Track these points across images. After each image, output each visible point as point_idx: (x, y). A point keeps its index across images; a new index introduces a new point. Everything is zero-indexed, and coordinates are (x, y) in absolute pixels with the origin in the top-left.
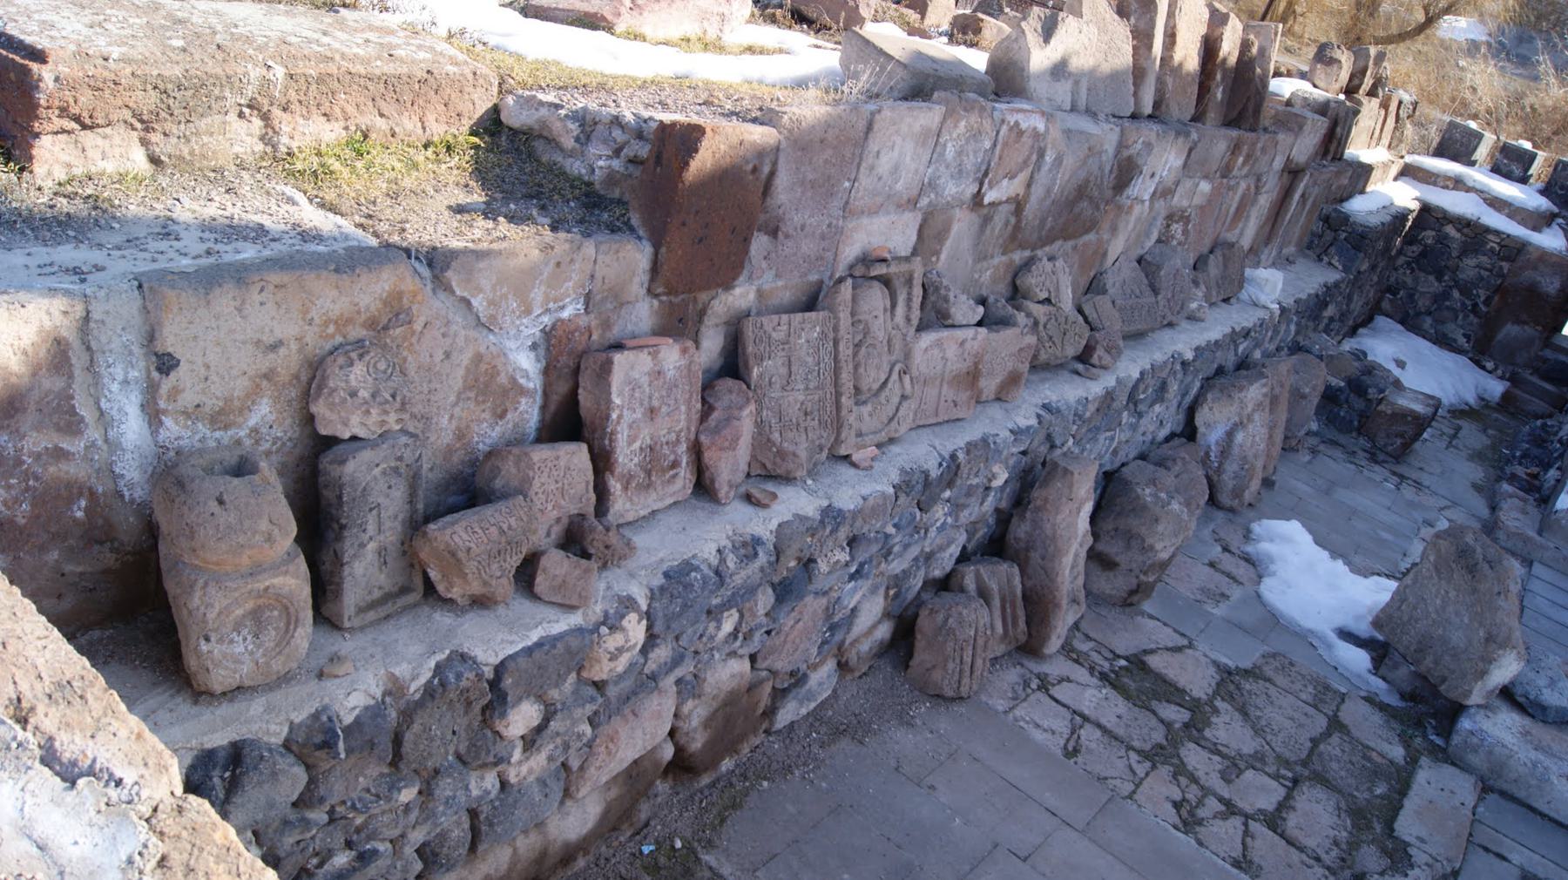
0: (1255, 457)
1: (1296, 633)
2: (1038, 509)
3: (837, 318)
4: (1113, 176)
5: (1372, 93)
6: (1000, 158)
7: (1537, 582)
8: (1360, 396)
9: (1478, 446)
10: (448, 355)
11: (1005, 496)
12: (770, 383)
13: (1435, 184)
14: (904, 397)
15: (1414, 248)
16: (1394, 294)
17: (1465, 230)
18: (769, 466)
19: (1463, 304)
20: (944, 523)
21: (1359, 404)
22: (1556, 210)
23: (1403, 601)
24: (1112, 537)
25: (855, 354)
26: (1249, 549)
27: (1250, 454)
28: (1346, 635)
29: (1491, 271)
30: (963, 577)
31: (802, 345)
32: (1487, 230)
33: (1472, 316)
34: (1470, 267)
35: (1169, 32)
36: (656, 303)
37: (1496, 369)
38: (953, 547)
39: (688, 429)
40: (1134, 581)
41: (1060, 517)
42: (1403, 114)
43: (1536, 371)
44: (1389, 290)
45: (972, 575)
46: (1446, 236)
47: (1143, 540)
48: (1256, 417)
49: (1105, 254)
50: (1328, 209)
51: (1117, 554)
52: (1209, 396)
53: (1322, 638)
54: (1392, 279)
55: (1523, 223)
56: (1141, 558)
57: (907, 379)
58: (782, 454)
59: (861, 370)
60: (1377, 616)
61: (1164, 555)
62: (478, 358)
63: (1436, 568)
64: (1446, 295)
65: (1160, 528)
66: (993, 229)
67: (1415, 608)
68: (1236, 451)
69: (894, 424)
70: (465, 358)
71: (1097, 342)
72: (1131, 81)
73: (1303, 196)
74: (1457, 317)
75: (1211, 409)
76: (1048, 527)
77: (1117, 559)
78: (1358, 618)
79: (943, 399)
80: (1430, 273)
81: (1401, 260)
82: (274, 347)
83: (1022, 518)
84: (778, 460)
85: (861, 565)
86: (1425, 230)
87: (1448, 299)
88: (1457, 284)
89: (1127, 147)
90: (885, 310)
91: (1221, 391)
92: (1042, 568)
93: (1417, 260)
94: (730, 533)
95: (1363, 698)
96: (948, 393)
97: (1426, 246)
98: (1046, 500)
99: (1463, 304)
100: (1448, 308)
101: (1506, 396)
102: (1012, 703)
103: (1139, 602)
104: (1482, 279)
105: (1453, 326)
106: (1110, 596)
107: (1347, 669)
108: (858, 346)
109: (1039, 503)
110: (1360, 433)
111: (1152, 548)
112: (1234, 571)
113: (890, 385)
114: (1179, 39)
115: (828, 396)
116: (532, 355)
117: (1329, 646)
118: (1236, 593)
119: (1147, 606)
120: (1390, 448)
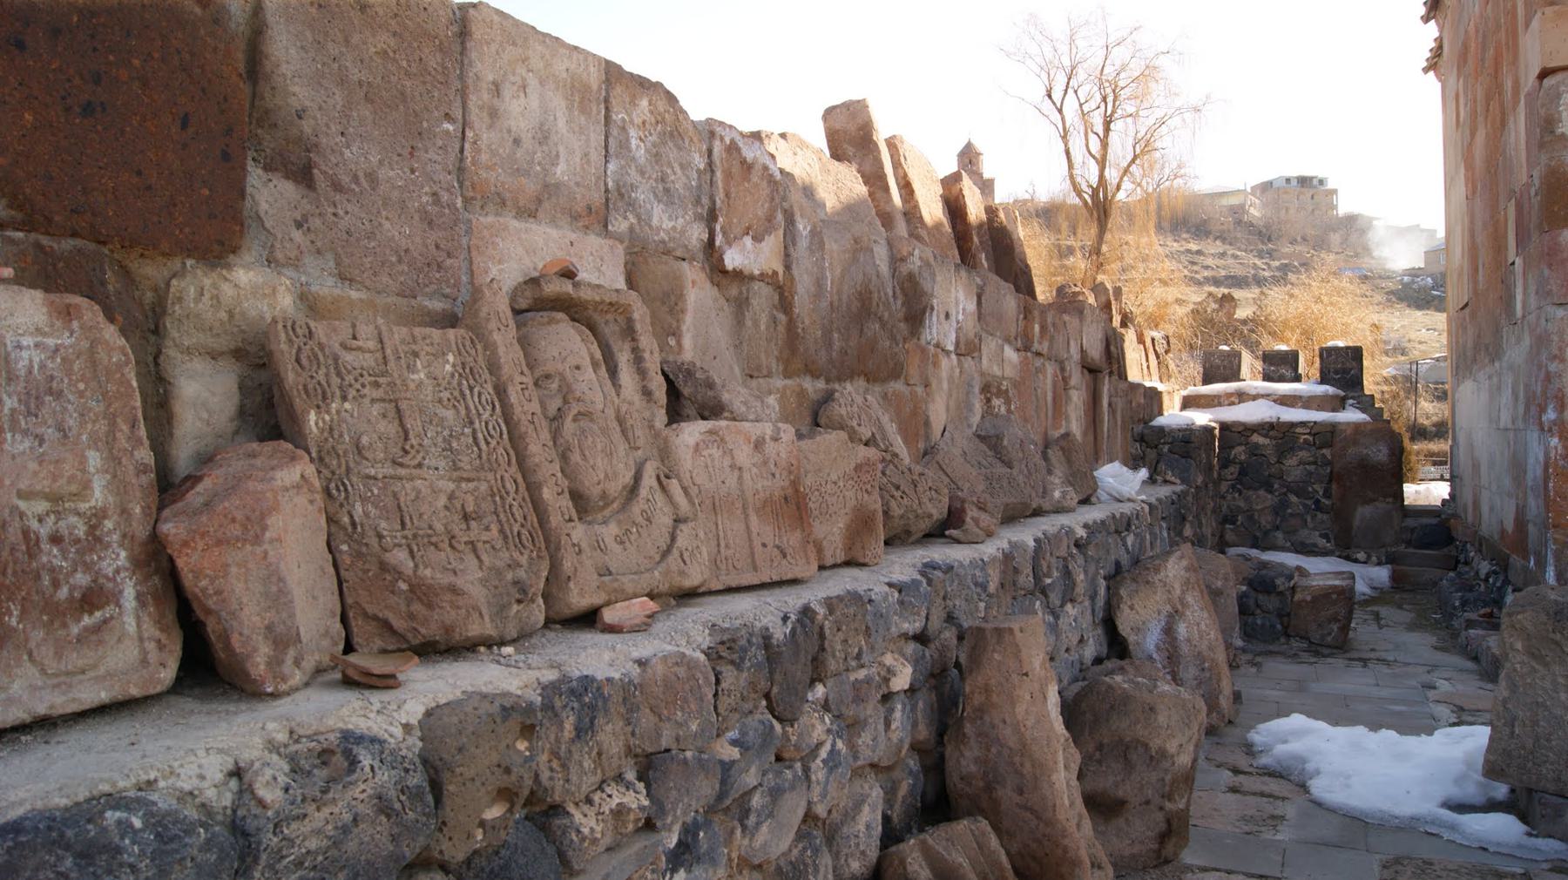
0: (1211, 648)
1: (1399, 829)
2: (981, 711)
3: (490, 347)
4: (899, 302)
5: (1124, 324)
6: (727, 195)
8: (1269, 593)
9: (1408, 620)
11: (920, 715)
12: (359, 449)
13: (1220, 405)
14: (677, 521)
15: (1232, 469)
16: (1234, 523)
17: (1271, 433)
18: (398, 624)
19: (1305, 506)
20: (833, 752)
21: (1271, 602)
22: (1342, 393)
23: (1511, 723)
24: (1099, 762)
25: (556, 435)
26: (1264, 760)
27: (1204, 647)
28: (1461, 808)
29: (1315, 463)
30: (903, 862)
31: (420, 385)
32: (1292, 425)
33: (1319, 515)
34: (1293, 466)
35: (903, 183)
37: (1369, 557)
38: (866, 809)
39: (124, 511)
40: (1160, 816)
41: (1020, 709)
42: (1161, 350)
43: (1409, 543)
44: (1225, 520)
45: (916, 854)
46: (1257, 446)
47: (1146, 746)
48: (1189, 599)
49: (927, 423)
50: (1139, 428)
51: (1116, 785)
52: (1123, 592)
53: (1434, 821)
54: (1224, 509)
55: (1320, 408)
56: (1154, 777)
57: (674, 486)
58: (421, 592)
59: (576, 457)
60: (1487, 761)
61: (1184, 759)
63: (1533, 655)
64: (1284, 504)
65: (1162, 719)
66: (756, 323)
67: (1535, 723)
68: (1185, 649)
69: (673, 560)
71: (963, 501)
72: (879, 223)
73: (1110, 405)
74: (1306, 521)
75: (1132, 608)
76: (1007, 732)
77: (1120, 793)
78: (1459, 780)
79: (757, 543)
80: (1260, 487)
81: (1224, 487)
83: (961, 738)
84: (417, 607)
85: (690, 832)
86: (1233, 447)
87: (1288, 507)
88: (1290, 490)
89: (903, 260)
90: (595, 365)
91: (1134, 580)
92: (1026, 808)
93: (1239, 480)
94: (282, 737)
95: (1551, 870)
96: (763, 530)
97: (1241, 463)
98: (987, 690)
99: (1305, 506)
100: (1291, 515)
101: (1395, 577)
103: (1176, 855)
104: (1310, 473)
105: (1306, 532)
106: (1133, 856)
107: (1499, 844)
108: (556, 419)
109: (978, 699)
110: (1288, 636)
111: (1163, 753)
112: (1266, 789)
113: (643, 492)
114: (916, 186)
115: (510, 486)
117: (1453, 827)
118: (1290, 810)
119: (1188, 857)
120: (1329, 639)
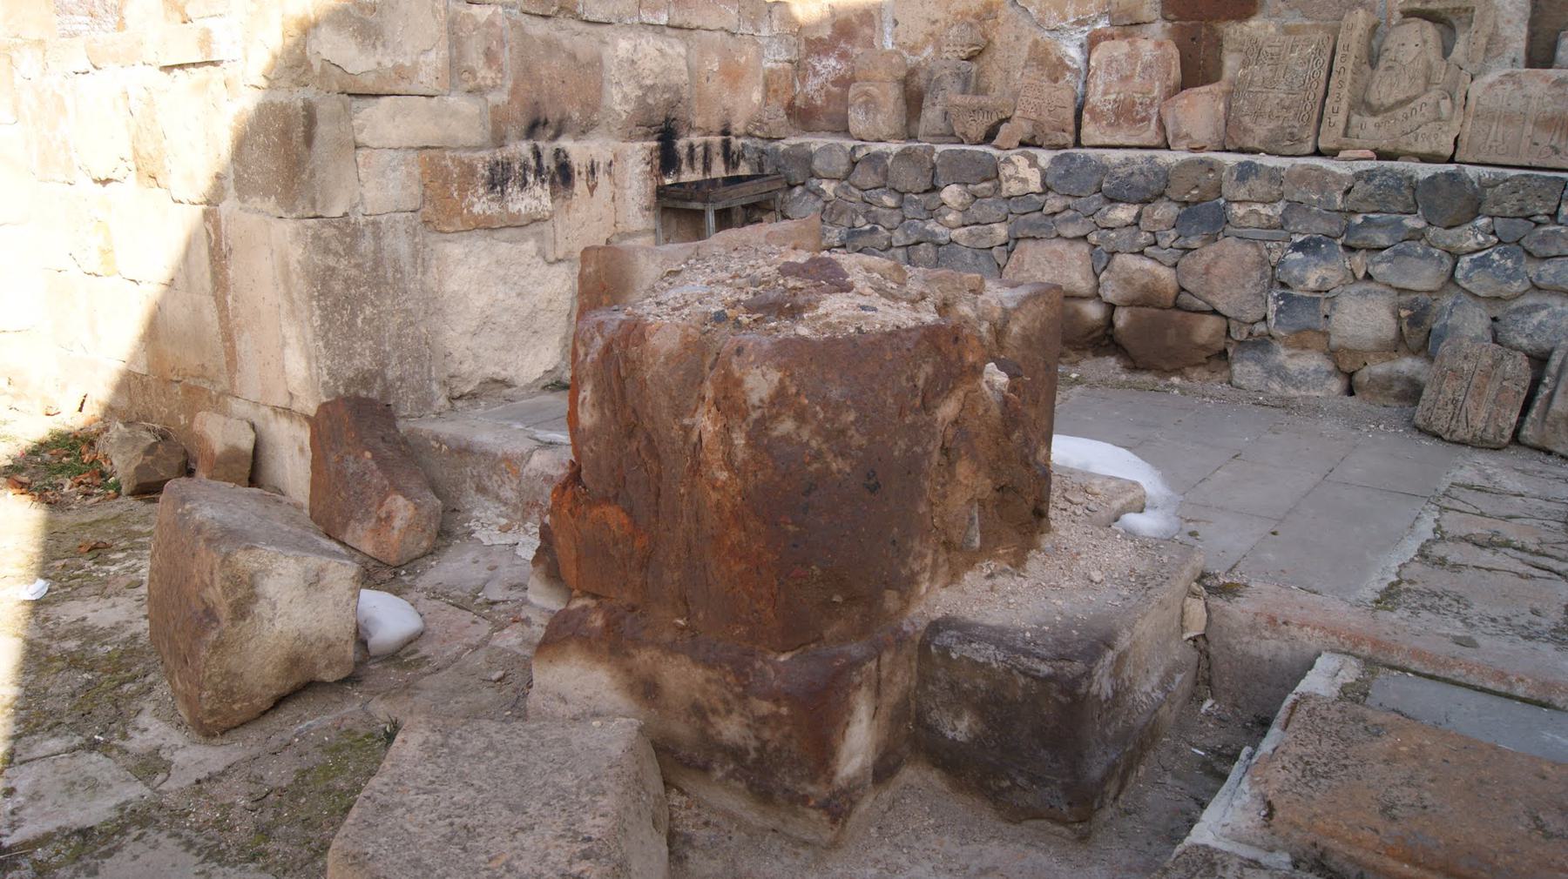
7: (1523, 288)
10: (1017, 38)
36: (1169, 25)
62: (1036, 43)
70: (1029, 42)
82: (934, 22)
102: (1114, 31)
116: (1079, 50)
